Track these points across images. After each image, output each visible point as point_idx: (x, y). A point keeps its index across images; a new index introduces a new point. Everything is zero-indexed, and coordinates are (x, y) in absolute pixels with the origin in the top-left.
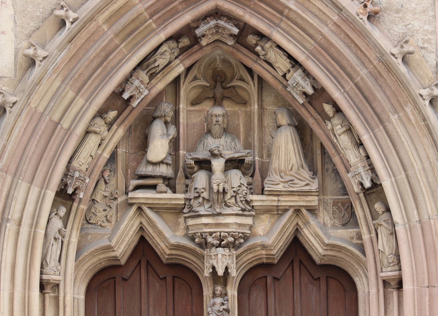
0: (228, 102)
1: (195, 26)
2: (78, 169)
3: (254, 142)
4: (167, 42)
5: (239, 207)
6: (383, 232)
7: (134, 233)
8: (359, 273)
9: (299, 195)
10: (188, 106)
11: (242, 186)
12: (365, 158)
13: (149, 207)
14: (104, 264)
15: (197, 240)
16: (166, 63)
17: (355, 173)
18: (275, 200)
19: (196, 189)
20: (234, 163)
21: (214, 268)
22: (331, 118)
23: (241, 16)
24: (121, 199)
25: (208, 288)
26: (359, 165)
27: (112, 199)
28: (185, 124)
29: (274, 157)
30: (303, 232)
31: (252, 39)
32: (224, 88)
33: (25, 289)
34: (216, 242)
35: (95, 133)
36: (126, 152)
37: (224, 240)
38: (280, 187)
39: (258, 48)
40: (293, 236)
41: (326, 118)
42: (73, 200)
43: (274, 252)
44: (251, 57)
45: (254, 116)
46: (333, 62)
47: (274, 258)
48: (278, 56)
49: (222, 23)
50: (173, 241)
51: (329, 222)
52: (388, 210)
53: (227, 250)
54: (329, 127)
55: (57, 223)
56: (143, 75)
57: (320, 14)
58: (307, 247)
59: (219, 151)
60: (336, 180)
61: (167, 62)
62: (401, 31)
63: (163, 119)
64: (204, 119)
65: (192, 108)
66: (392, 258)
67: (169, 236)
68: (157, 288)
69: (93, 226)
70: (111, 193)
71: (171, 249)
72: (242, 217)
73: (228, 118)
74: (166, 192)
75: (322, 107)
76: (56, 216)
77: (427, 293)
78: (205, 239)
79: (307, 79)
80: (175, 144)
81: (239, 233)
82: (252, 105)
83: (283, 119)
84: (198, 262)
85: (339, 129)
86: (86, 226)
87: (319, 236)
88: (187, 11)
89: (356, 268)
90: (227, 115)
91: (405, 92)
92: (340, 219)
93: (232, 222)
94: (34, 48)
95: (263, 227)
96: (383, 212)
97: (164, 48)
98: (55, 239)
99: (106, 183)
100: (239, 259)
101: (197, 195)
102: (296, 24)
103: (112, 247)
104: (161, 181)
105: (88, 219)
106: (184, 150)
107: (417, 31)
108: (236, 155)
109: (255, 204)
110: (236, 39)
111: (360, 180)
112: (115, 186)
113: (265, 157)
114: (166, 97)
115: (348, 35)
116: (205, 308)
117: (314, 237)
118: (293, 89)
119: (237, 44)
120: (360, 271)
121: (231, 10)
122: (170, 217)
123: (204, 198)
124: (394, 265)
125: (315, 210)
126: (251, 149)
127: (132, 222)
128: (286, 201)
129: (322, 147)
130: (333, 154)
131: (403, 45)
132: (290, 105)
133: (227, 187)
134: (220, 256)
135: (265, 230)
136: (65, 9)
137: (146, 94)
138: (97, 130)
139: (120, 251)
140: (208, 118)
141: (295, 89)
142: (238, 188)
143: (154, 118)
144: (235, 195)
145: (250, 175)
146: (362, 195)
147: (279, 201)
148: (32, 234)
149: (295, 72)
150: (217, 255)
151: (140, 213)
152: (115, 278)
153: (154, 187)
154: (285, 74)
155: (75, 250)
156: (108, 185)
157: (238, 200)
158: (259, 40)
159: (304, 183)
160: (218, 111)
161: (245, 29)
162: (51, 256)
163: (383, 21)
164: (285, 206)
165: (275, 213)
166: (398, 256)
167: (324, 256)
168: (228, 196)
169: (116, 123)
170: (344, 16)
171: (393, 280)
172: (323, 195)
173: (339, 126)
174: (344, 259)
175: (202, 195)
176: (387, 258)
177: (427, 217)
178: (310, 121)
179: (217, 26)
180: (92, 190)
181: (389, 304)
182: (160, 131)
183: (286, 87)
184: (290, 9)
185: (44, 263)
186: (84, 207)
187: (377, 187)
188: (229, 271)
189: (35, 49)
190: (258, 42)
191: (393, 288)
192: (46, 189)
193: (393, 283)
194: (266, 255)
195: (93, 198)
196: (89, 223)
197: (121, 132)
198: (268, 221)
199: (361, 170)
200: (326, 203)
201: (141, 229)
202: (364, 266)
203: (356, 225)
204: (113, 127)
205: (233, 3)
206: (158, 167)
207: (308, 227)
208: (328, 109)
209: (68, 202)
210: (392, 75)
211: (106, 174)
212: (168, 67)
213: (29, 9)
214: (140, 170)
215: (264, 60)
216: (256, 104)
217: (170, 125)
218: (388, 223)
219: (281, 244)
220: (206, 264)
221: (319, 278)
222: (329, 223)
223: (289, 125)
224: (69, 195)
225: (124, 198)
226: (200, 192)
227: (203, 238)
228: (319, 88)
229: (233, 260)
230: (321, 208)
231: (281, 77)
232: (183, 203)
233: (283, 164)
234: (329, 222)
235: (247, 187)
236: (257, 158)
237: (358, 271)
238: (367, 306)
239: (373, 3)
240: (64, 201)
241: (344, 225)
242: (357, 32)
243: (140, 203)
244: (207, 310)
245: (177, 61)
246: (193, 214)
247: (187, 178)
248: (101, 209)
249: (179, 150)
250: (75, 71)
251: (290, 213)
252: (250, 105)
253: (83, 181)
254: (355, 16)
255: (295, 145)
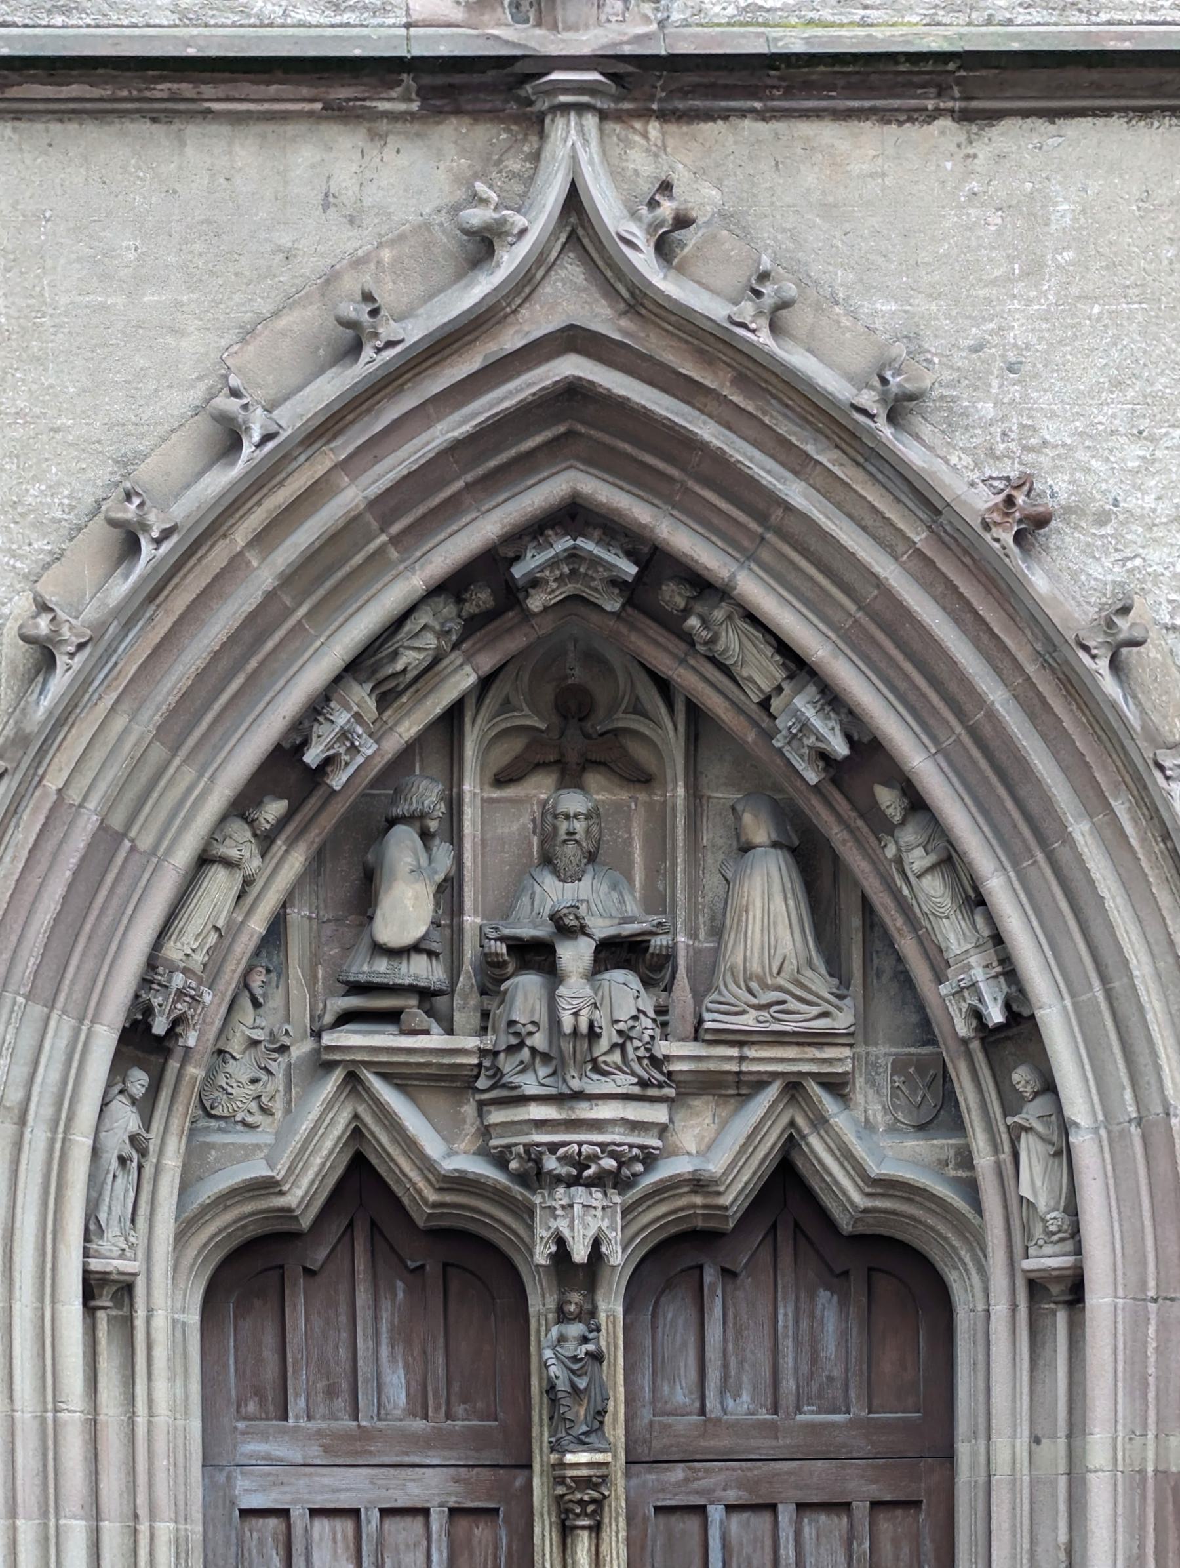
0: (599, 777)
1: (511, 555)
2: (182, 965)
3: (673, 895)
4: (430, 601)
5: (633, 1074)
6: (1032, 1151)
7: (336, 1145)
8: (961, 1259)
9: (798, 1044)
10: (486, 787)
11: (641, 1016)
12: (990, 944)
13: (378, 1074)
14: (252, 1232)
15: (513, 1165)
16: (425, 664)
17: (962, 984)
18: (730, 1058)
19: (512, 1023)
20: (618, 952)
21: (560, 1241)
22: (896, 826)
23: (645, 526)
24: (301, 1049)
25: (543, 1295)
26: (973, 960)
27: (274, 1050)
28: (478, 840)
29: (731, 938)
30: (808, 1144)
31: (673, 595)
32: (587, 736)
33: (41, 1299)
34: (564, 1170)
35: (228, 863)
36: (310, 918)
37: (589, 1167)
38: (748, 1021)
39: (693, 622)
40: (779, 1158)
41: (882, 826)
42: (167, 1053)
43: (726, 1200)
44: (670, 646)
45: (674, 817)
46: (908, 667)
47: (727, 1217)
48: (749, 645)
49: (588, 545)
50: (449, 1165)
51: (879, 1118)
52: (1049, 1087)
53: (597, 1194)
54: (891, 851)
55: (126, 1118)
56: (361, 695)
57: (877, 524)
58: (817, 1188)
59: (577, 918)
60: (904, 1003)
61: (430, 659)
62: (1109, 578)
63: (417, 824)
64: (531, 826)
65: (496, 794)
66: (1056, 1219)
67: (437, 1146)
68: (400, 1295)
69: (222, 1124)
70: (272, 1033)
71: (441, 1189)
72: (640, 1104)
73: (599, 824)
74: (427, 1032)
75: (872, 795)
76: (121, 1098)
77: (1153, 1317)
78: (538, 1162)
79: (832, 715)
80: (449, 893)
81: (631, 1146)
82: (670, 787)
83: (760, 831)
84: (515, 1225)
85: (918, 859)
86: (203, 1123)
87: (852, 1155)
88: (489, 510)
89: (953, 1247)
90: (598, 815)
91: (1115, 756)
92: (910, 1112)
93: (613, 1114)
94: (51, 616)
95: (697, 1130)
96: (1036, 1094)
97: (424, 617)
98: (123, 1161)
99: (256, 1004)
100: (630, 1217)
101: (514, 1041)
102: (804, 552)
103: (277, 1184)
104: (413, 1002)
105: (207, 1105)
106: (476, 913)
107: (1157, 576)
108: (629, 929)
109: (676, 1067)
110: (627, 594)
111: (976, 1003)
112: (281, 1013)
113: (702, 936)
114: (422, 761)
115: (955, 588)
116: (533, 1348)
117: (837, 1159)
118: (789, 743)
119: (629, 609)
120: (963, 1253)
121: (617, 509)
122: (440, 1103)
123: (533, 1050)
124: (1062, 1240)
125: (845, 1084)
126: (664, 912)
127: (331, 1115)
128: (762, 1059)
129: (867, 907)
130: (899, 930)
131: (1115, 619)
132: (777, 787)
133: (601, 1019)
134: (577, 1209)
135: (703, 1138)
136: (137, 501)
137: (369, 752)
138: (233, 853)
139: (299, 1192)
140: (549, 815)
141: (795, 743)
142: (631, 1023)
143: (392, 822)
144: (620, 1041)
145: (662, 985)
146: (975, 1045)
147: (742, 1059)
148: (58, 1145)
149: (797, 692)
150: (571, 1206)
151: (354, 1090)
152: (282, 1267)
153: (391, 1017)
154: (769, 698)
155: (176, 1191)
156: (261, 1011)
157: (631, 1055)
158: (694, 598)
159: (815, 1011)
160: (574, 802)
161: (655, 560)
162: (110, 1207)
163: (1058, 548)
164: (759, 1072)
165: (731, 1092)
166: (1072, 1209)
167: (866, 1211)
168: (604, 1044)
169: (283, 836)
170: (945, 531)
171: (1059, 1279)
172: (866, 1044)
173: (919, 852)
174: (920, 1222)
175: (529, 1042)
176: (1044, 1220)
177: (1160, 1110)
178: (837, 835)
179: (573, 555)
180: (218, 1023)
181: (1044, 1344)
182: (409, 860)
183: (768, 735)
184: (788, 508)
185: (92, 1227)
186: (195, 1071)
187: (1018, 1024)
188: (604, 1249)
189: (54, 619)
190: (692, 602)
191: (1056, 1303)
192: (92, 1022)
193: (1055, 1289)
194: (705, 1207)
195: (220, 1045)
196: (210, 1116)
197: (296, 861)
198: (710, 1114)
199: (979, 974)
200: (875, 1065)
201: (357, 1133)
202: (976, 1239)
203: (958, 1126)
204: (275, 848)
205: (622, 488)
206: (405, 963)
207: (822, 1132)
208: (887, 798)
209: (153, 1058)
210: (1079, 708)
211: (257, 981)
212: (431, 674)
213: (30, 500)
214: (354, 969)
215: (708, 658)
216: (681, 783)
217: (437, 841)
218: (1048, 1125)
219: (745, 1179)
220: (541, 1232)
221: (846, 1273)
222: (880, 1118)
223: (775, 845)
224: (158, 1038)
225: (308, 1045)
226: (524, 1031)
227: (530, 1160)
228: (866, 740)
229: (613, 1221)
230: (860, 1081)
231: (754, 707)
232: (476, 1061)
233: (756, 955)
234: (879, 1118)
235: (654, 1020)
236: (681, 938)
237: (958, 1255)
238: (981, 1349)
239: (1033, 494)
240: (140, 1055)
241: (921, 1127)
242: (983, 579)
243: (354, 1062)
244: (540, 1355)
245: (456, 657)
246: (505, 1093)
247: (483, 992)
248: (245, 1079)
249: (461, 911)
250: (169, 685)
251: (773, 1091)
252: (664, 785)
253: (196, 1000)
254: (980, 531)
255: (791, 903)
